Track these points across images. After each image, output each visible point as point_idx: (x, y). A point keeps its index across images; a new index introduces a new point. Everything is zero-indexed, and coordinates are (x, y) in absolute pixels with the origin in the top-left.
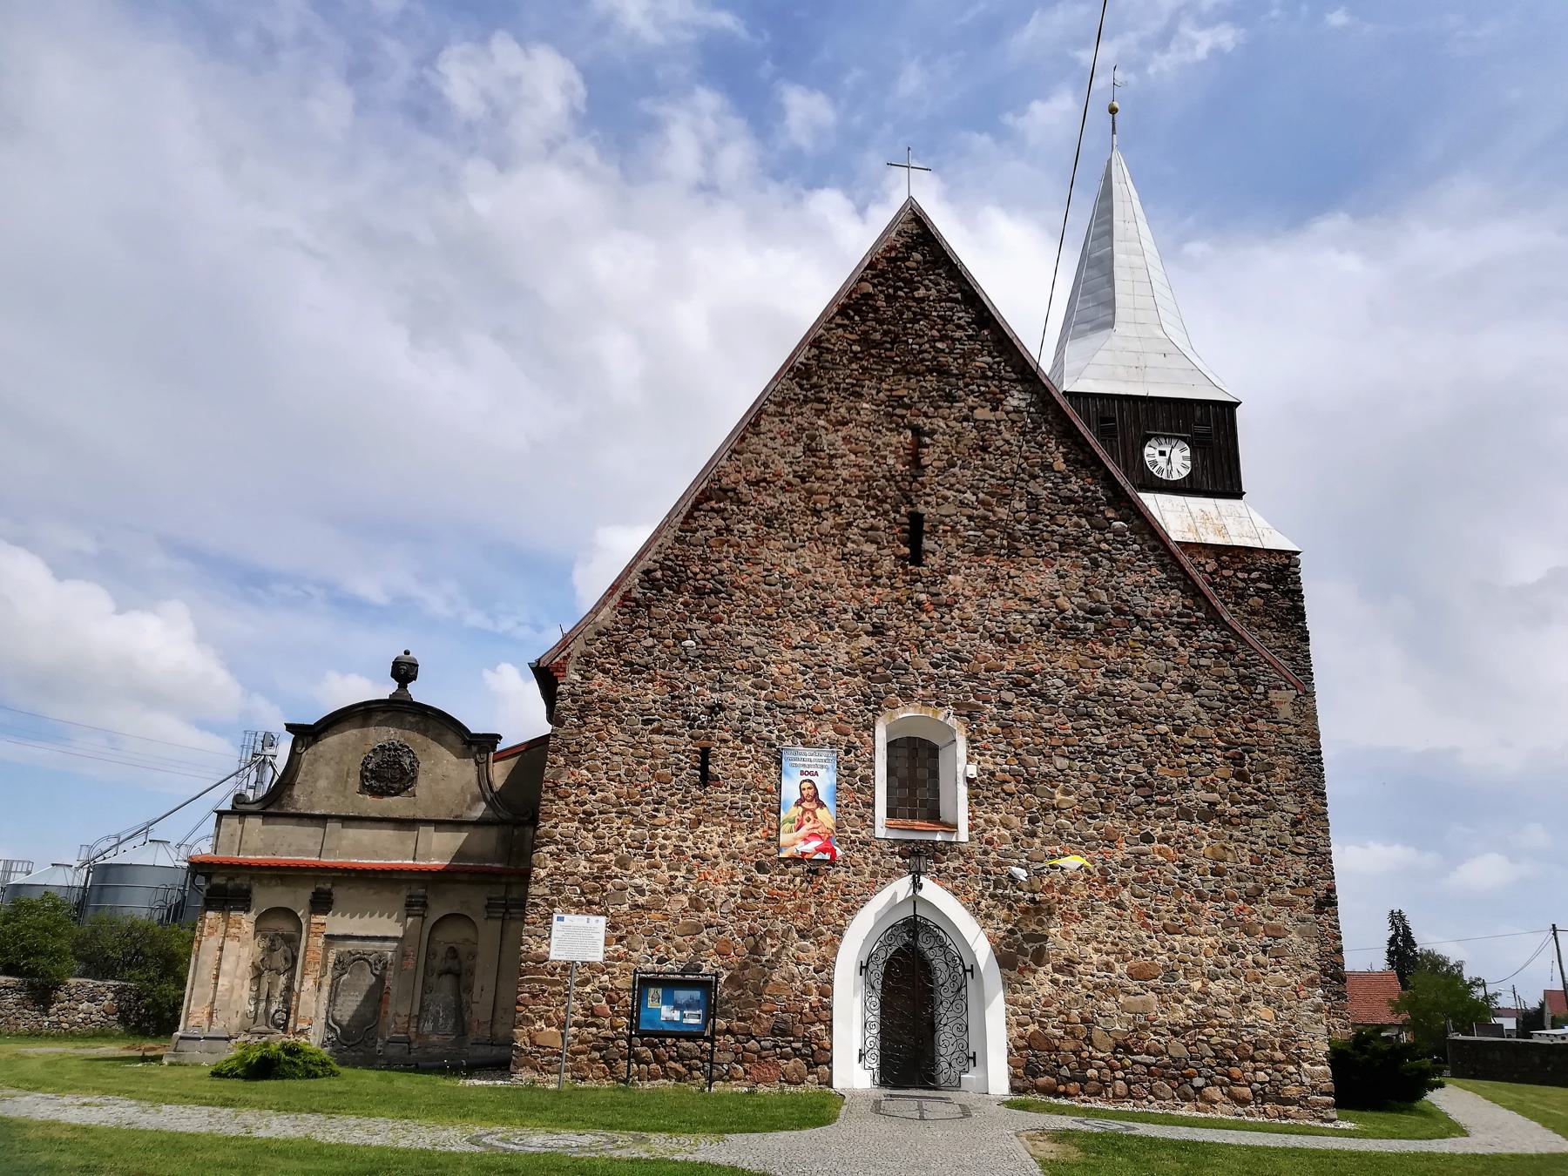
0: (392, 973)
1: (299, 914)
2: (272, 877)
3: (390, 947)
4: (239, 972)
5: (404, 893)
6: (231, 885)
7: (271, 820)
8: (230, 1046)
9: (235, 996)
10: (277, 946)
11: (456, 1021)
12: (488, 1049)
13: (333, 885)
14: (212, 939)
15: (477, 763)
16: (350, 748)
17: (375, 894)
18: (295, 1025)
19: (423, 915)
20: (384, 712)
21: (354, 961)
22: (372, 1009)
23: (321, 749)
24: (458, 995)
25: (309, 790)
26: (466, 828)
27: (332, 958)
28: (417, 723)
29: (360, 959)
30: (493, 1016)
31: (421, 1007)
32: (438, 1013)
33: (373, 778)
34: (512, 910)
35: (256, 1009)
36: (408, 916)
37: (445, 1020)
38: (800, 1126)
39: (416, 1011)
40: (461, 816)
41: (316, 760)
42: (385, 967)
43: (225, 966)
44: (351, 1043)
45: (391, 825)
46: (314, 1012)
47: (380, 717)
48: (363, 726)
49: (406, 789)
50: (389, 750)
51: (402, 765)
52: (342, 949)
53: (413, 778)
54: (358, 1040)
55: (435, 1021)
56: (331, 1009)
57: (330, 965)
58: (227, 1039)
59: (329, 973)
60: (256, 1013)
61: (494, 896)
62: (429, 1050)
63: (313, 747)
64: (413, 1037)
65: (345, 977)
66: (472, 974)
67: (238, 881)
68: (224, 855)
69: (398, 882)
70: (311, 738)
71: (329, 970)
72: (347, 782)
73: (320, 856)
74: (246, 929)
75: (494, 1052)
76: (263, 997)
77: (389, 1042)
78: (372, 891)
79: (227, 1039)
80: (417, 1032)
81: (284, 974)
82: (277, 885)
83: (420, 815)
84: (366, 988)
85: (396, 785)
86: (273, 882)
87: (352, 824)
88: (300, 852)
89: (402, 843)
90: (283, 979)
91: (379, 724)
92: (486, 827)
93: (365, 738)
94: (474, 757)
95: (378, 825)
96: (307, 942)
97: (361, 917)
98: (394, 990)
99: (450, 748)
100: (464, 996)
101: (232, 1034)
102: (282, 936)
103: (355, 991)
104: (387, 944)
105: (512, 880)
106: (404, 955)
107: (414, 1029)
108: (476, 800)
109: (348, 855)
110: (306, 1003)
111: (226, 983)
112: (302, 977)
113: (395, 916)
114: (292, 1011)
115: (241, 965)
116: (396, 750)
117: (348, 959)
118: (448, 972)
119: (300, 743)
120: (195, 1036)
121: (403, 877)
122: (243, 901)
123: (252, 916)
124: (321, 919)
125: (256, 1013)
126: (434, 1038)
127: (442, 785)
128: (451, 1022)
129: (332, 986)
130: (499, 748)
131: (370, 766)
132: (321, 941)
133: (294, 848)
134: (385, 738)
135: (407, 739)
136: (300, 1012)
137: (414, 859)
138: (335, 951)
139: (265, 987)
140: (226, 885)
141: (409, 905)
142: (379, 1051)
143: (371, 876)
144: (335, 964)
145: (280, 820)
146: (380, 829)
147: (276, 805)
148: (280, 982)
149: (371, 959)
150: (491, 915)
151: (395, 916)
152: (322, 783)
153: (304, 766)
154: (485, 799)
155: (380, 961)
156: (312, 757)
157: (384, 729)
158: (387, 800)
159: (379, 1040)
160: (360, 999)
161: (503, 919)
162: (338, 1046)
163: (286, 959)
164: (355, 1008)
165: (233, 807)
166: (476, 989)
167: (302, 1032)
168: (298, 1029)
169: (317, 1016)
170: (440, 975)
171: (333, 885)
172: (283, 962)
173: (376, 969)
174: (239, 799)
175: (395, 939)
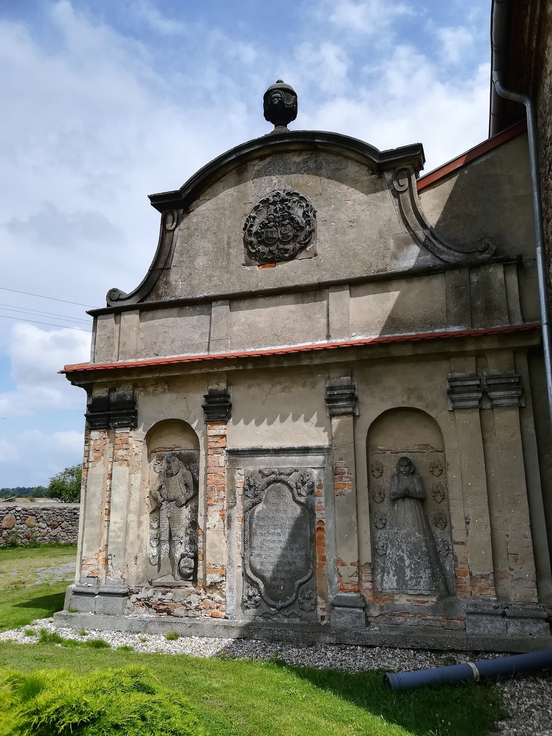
0: (322, 499)
1: (194, 426)
2: (157, 382)
3: (315, 462)
4: (133, 505)
5: (322, 386)
6: (114, 397)
7: (150, 315)
8: (129, 603)
9: (132, 537)
10: (174, 470)
11: (433, 574)
12: (499, 623)
13: (229, 384)
14: (99, 464)
15: (396, 194)
16: (227, 213)
17: (283, 390)
18: (205, 576)
19: (353, 414)
20: (262, 158)
21: (269, 484)
22: (303, 553)
23: (194, 220)
24: (428, 532)
25: (187, 271)
26: (395, 285)
27: (240, 481)
28: (305, 162)
29: (276, 481)
30: (495, 565)
31: (374, 551)
32: (402, 559)
33: (260, 243)
34: (493, 394)
35: (159, 552)
36: (332, 416)
37: (415, 571)
38: (548, 545)
39: (367, 557)
40: (385, 269)
41: (190, 235)
42: (311, 492)
43: (117, 499)
44: (280, 604)
45: (291, 298)
46: (226, 558)
47: (258, 165)
48: (239, 182)
49: (303, 248)
50: (274, 203)
51: (292, 219)
52: (251, 469)
53: (310, 233)
54: (290, 600)
55: (400, 572)
56: (247, 554)
57: (239, 491)
58: (126, 595)
59: (239, 503)
60: (159, 558)
61: (457, 375)
62: (400, 620)
63: (185, 221)
64: (369, 597)
65: (259, 508)
66: (444, 497)
67: (120, 392)
68: (101, 363)
69: (311, 370)
70: (181, 211)
71: (239, 498)
72: (229, 254)
73: (208, 350)
74: (137, 450)
75: (512, 630)
76: (165, 537)
77: (333, 605)
78: (278, 388)
79: (126, 595)
80: (374, 589)
81: (186, 504)
82: (164, 392)
83: (327, 278)
84: (289, 523)
85: (290, 247)
86: (160, 389)
87: (242, 304)
88: (185, 347)
89: (309, 318)
90: (186, 512)
91: (258, 175)
92: (425, 280)
93: (243, 196)
94: (390, 185)
95: (274, 300)
96: (207, 461)
97: (270, 423)
98: (329, 526)
99: (354, 183)
100: (437, 531)
101: (133, 587)
102: (180, 457)
103: (275, 526)
104: (310, 458)
105: (485, 346)
106: (336, 473)
107: (368, 585)
108: (402, 244)
109: (241, 344)
110: (213, 545)
111: (118, 520)
112: (206, 509)
113: (314, 419)
114: (200, 557)
115: (133, 496)
116: (283, 201)
117: (261, 482)
118: (406, 496)
119: (170, 218)
120: (90, 590)
121: (316, 362)
122: (128, 414)
123: (141, 433)
124: (217, 430)
125: (159, 558)
126: (403, 601)
127: (351, 234)
128: (425, 575)
129: (244, 520)
130: (428, 168)
131: (254, 229)
132: (222, 459)
133: (178, 344)
134: (268, 190)
135: (296, 185)
136: (209, 558)
137: (328, 337)
138: (242, 472)
139: (165, 524)
140: (108, 398)
141: (330, 400)
142: (323, 618)
143: (272, 365)
144: (245, 490)
145: (159, 313)
146: (277, 305)
147: (153, 296)
148: (183, 517)
149: (292, 480)
150: (457, 404)
151: (314, 419)
152: (201, 261)
153: (178, 244)
154: (416, 240)
155: (303, 483)
156: (186, 232)
157: (265, 180)
158: (281, 267)
159: (319, 600)
160: (284, 538)
161: (481, 410)
162: (265, 609)
163: (186, 485)
164: (279, 552)
165: (108, 305)
166: (457, 523)
167: (214, 586)
168: (209, 581)
169: (230, 563)
170: (394, 501)
171: (229, 384)
172: (184, 490)
173: (300, 495)
174: (113, 295)
175: (319, 450)
